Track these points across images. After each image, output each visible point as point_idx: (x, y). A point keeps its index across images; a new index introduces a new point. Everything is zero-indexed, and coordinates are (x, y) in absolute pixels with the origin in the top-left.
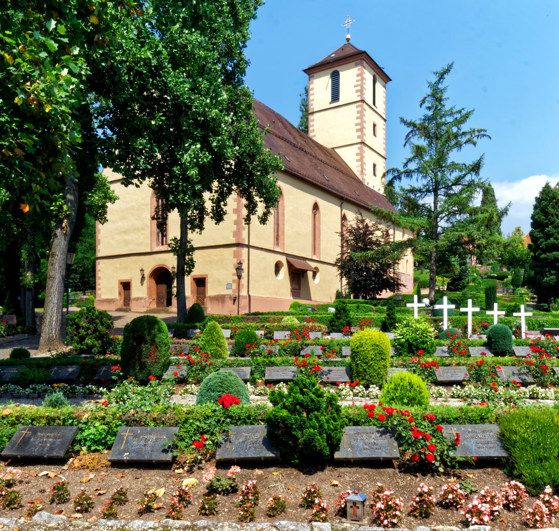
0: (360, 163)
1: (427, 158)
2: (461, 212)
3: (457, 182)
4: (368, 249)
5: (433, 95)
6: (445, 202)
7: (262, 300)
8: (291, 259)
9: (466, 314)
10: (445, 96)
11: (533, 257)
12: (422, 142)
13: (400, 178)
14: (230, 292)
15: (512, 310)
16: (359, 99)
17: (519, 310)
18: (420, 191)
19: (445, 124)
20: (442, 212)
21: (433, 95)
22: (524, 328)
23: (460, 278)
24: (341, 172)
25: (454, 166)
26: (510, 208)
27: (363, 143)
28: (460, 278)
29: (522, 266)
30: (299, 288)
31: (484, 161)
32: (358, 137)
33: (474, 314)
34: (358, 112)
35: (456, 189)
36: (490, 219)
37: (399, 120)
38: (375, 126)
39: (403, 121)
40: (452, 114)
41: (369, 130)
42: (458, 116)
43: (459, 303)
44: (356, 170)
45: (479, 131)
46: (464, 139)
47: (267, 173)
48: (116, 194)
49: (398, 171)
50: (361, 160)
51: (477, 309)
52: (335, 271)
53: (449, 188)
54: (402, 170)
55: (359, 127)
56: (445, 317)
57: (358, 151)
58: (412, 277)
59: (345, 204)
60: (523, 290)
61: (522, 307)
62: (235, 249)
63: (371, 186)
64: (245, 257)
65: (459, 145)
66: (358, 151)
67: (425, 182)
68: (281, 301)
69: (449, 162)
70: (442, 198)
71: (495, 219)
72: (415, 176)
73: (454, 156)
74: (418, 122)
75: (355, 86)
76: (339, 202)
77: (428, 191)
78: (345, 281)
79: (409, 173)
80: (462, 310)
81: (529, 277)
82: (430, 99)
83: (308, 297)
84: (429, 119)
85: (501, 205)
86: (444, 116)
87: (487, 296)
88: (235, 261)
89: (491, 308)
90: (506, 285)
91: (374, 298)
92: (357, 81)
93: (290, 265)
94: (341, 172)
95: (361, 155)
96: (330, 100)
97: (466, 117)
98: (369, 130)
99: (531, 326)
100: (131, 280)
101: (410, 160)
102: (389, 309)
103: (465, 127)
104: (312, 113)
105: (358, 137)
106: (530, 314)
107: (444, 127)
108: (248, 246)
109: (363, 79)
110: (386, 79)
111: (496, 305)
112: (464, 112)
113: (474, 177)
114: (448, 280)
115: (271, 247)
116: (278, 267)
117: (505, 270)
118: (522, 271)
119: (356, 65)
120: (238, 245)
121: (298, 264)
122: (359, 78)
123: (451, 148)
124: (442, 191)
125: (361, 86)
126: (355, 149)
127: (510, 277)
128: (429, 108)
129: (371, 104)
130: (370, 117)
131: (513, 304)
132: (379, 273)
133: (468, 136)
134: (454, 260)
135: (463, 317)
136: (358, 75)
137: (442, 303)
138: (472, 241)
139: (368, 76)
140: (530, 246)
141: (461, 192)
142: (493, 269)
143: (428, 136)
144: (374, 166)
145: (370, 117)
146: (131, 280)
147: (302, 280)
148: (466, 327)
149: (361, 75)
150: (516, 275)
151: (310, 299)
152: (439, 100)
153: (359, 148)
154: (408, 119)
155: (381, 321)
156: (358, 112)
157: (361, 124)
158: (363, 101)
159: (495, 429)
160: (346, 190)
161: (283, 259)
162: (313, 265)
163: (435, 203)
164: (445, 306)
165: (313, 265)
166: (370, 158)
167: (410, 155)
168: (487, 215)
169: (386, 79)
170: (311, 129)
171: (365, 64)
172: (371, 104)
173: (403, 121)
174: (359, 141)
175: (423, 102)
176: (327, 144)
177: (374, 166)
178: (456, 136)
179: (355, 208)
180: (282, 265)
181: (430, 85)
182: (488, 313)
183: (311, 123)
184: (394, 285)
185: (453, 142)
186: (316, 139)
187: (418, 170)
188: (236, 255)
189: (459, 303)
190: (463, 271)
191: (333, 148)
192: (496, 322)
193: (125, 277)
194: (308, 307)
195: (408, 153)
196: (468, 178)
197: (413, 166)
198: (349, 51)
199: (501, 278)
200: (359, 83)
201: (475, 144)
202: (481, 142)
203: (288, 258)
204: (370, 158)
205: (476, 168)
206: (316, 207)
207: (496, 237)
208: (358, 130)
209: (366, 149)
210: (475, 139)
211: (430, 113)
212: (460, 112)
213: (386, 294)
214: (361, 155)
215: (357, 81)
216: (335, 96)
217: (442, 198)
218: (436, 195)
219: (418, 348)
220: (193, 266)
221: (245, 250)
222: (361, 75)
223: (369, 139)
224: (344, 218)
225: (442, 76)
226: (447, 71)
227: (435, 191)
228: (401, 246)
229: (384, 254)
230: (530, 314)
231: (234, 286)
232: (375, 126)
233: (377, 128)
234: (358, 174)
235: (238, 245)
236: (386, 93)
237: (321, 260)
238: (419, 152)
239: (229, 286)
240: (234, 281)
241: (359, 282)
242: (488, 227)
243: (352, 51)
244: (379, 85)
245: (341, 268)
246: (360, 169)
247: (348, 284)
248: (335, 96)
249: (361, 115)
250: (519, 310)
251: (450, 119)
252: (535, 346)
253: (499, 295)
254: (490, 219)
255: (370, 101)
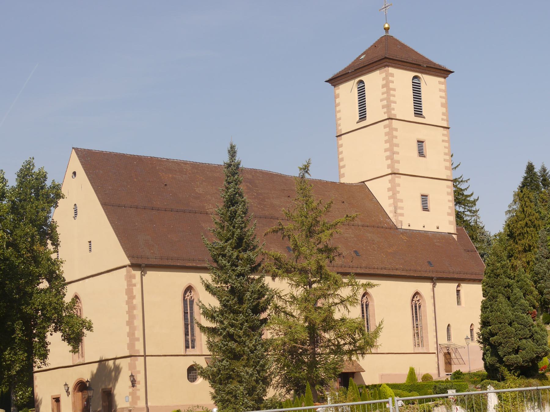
0: (391, 201)
26: (376, 287)
48: (275, 280)
57: (389, 186)
66: (389, 186)
75: (382, 100)
92: (383, 94)
96: (358, 118)
100: (60, 395)
105: (389, 166)
122: (385, 89)
146: (60, 395)
153: (390, 181)
155: (507, 379)
193: (56, 394)
194: (365, 308)
200: (385, 96)
215: (383, 94)
216: (363, 117)
246: (392, 208)
248: (363, 117)
249: (390, 137)
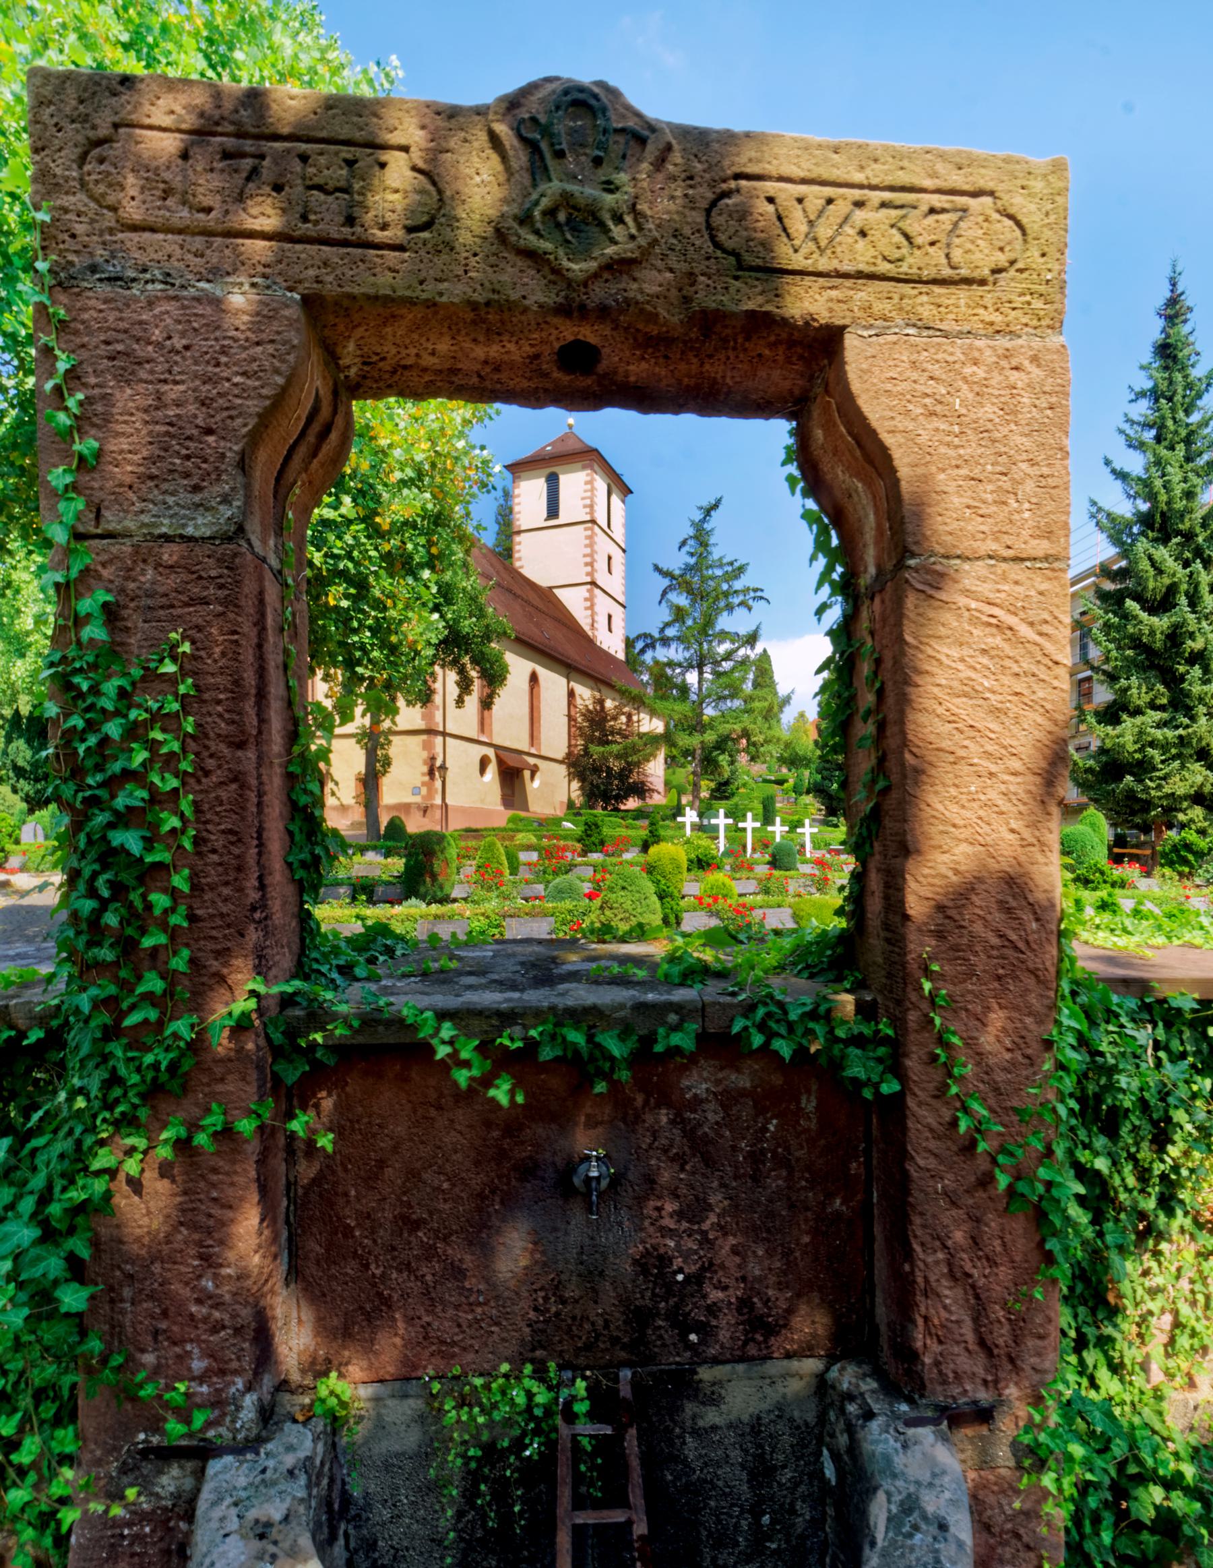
1: (689, 622)
2: (732, 696)
3: (728, 656)
4: (608, 743)
5: (695, 537)
6: (712, 682)
7: (464, 811)
8: (500, 752)
9: (744, 830)
10: (712, 540)
11: (820, 757)
12: (682, 600)
13: (654, 647)
14: (417, 799)
15: (795, 825)
16: (588, 518)
17: (803, 826)
18: (680, 665)
19: (712, 578)
20: (709, 696)
21: (695, 537)
22: (808, 846)
23: (727, 783)
24: (565, 625)
25: (724, 636)
27: (593, 584)
28: (727, 783)
29: (807, 766)
30: (513, 795)
31: (761, 632)
32: (588, 574)
33: (754, 830)
34: (587, 537)
35: (726, 665)
36: (770, 709)
37: (651, 568)
38: (610, 558)
39: (657, 568)
40: (721, 566)
41: (601, 565)
42: (730, 569)
43: (736, 814)
44: (585, 623)
45: (755, 590)
46: (736, 600)
47: (490, 641)
49: (651, 637)
50: (591, 607)
51: (758, 825)
52: (562, 770)
53: (717, 663)
54: (657, 635)
55: (588, 560)
56: (722, 834)
58: (662, 779)
59: (573, 674)
60: (808, 799)
61: (807, 822)
62: (424, 737)
63: (605, 647)
64: (439, 750)
65: (730, 608)
67: (687, 655)
68: (489, 813)
69: (718, 628)
70: (708, 676)
71: (776, 709)
72: (674, 646)
73: (724, 622)
74: (677, 572)
76: (563, 670)
77: (691, 666)
78: (575, 785)
79: (666, 642)
80: (741, 825)
81: (816, 784)
82: (691, 542)
83: (526, 808)
84: (689, 568)
85: (782, 690)
86: (711, 566)
87: (765, 807)
88: (425, 755)
89: (773, 823)
90: (786, 792)
91: (617, 810)
93: (500, 762)
94: (565, 625)
95: (591, 599)
96: (545, 515)
97: (741, 570)
98: (601, 565)
99: (816, 846)
101: (667, 625)
102: (652, 824)
103: (738, 585)
104: (519, 532)
105: (588, 574)
106: (815, 830)
107: (711, 583)
108: (444, 734)
109: (593, 489)
110: (626, 491)
111: (778, 820)
112: (736, 565)
113: (749, 652)
114: (713, 785)
115: (473, 733)
116: (484, 763)
117: (784, 770)
118: (807, 773)
119: (584, 468)
120: (430, 732)
121: (512, 761)
123: (718, 612)
124: (708, 669)
125: (592, 499)
126: (583, 591)
127: (791, 782)
128: (692, 555)
129: (605, 527)
130: (604, 546)
131: (796, 818)
132: (624, 774)
133: (741, 598)
134: (723, 759)
135: (740, 834)
136: (586, 483)
137: (717, 817)
138: (746, 734)
139: (601, 485)
140: (816, 742)
141: (733, 669)
142: (769, 769)
143: (690, 591)
144: (610, 617)
145: (604, 546)
147: (517, 782)
148: (744, 847)
149: (590, 482)
150: (799, 779)
151: (527, 810)
152: (704, 544)
154: (664, 566)
156: (587, 537)
157: (591, 555)
158: (593, 522)
159: (790, 911)
160: (572, 652)
161: (491, 752)
162: (532, 761)
163: (700, 682)
164: (721, 821)
165: (532, 761)
166: (604, 605)
167: (668, 618)
168: (766, 704)
169: (626, 491)
170: (516, 555)
171: (596, 467)
172: (605, 527)
173: (657, 568)
174: (588, 579)
175: (683, 543)
176: (543, 581)
177: (610, 617)
178: (726, 594)
179: (591, 683)
180: (489, 761)
181: (693, 524)
182: (770, 828)
183: (517, 548)
184: (641, 790)
185: (722, 604)
186: (526, 572)
187: (678, 639)
188: (427, 746)
189: (736, 814)
190: (733, 772)
191: (551, 588)
192: (778, 839)
195: (665, 615)
196: (742, 652)
197: (671, 632)
198: (571, 446)
199: (780, 782)
201: (750, 609)
202: (757, 606)
203: (500, 752)
204: (604, 605)
205: (752, 639)
206: (534, 678)
207: (776, 732)
208: (586, 564)
209: (597, 591)
210: (751, 602)
211: (692, 561)
212: (731, 564)
213: (632, 803)
214: (591, 599)
217: (708, 676)
218: (701, 673)
219: (709, 865)
220: (389, 764)
221: (439, 739)
222: (590, 482)
223: (602, 578)
224: (571, 694)
225: (708, 511)
226: (715, 506)
227: (700, 667)
228: (653, 740)
229: (635, 750)
230: (815, 830)
231: (424, 791)
232: (610, 558)
233: (613, 561)
234: (587, 628)
235: (430, 732)
236: (627, 511)
237: (543, 753)
238: (679, 615)
239: (416, 791)
240: (424, 784)
241: (598, 787)
242: (766, 718)
243: (577, 446)
244: (615, 499)
245: (569, 766)
246: (589, 621)
247: (581, 788)
250: (803, 826)
251: (719, 572)
252: (820, 863)
253: (778, 805)
254: (770, 709)
255: (603, 522)
